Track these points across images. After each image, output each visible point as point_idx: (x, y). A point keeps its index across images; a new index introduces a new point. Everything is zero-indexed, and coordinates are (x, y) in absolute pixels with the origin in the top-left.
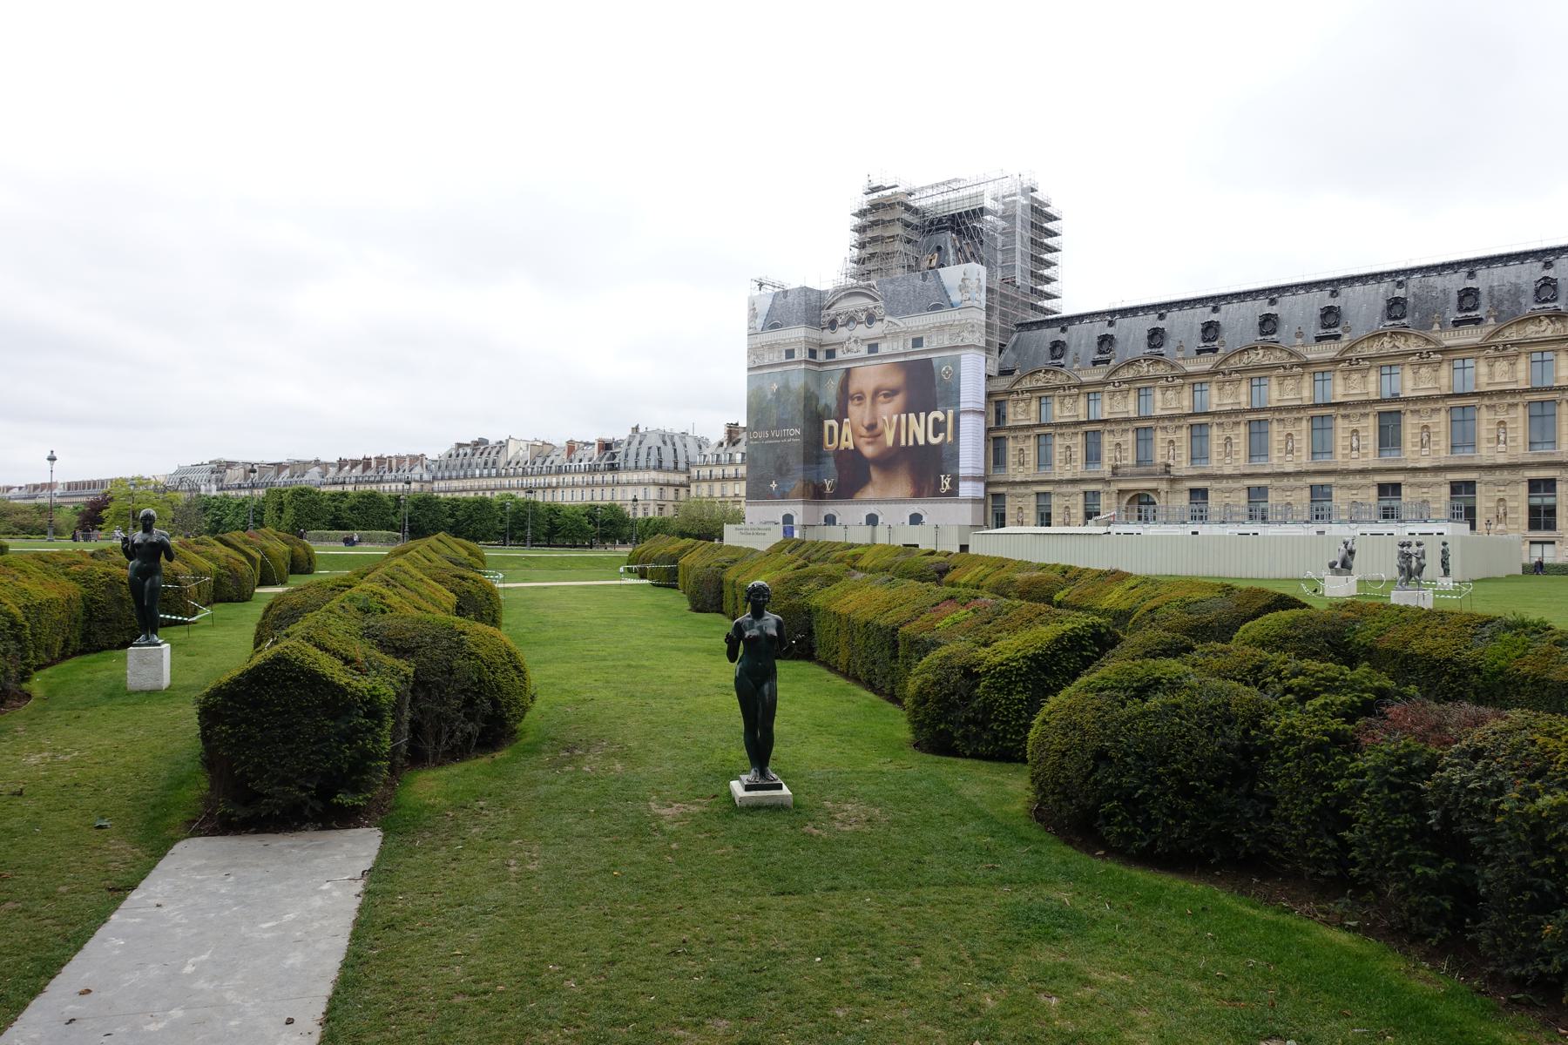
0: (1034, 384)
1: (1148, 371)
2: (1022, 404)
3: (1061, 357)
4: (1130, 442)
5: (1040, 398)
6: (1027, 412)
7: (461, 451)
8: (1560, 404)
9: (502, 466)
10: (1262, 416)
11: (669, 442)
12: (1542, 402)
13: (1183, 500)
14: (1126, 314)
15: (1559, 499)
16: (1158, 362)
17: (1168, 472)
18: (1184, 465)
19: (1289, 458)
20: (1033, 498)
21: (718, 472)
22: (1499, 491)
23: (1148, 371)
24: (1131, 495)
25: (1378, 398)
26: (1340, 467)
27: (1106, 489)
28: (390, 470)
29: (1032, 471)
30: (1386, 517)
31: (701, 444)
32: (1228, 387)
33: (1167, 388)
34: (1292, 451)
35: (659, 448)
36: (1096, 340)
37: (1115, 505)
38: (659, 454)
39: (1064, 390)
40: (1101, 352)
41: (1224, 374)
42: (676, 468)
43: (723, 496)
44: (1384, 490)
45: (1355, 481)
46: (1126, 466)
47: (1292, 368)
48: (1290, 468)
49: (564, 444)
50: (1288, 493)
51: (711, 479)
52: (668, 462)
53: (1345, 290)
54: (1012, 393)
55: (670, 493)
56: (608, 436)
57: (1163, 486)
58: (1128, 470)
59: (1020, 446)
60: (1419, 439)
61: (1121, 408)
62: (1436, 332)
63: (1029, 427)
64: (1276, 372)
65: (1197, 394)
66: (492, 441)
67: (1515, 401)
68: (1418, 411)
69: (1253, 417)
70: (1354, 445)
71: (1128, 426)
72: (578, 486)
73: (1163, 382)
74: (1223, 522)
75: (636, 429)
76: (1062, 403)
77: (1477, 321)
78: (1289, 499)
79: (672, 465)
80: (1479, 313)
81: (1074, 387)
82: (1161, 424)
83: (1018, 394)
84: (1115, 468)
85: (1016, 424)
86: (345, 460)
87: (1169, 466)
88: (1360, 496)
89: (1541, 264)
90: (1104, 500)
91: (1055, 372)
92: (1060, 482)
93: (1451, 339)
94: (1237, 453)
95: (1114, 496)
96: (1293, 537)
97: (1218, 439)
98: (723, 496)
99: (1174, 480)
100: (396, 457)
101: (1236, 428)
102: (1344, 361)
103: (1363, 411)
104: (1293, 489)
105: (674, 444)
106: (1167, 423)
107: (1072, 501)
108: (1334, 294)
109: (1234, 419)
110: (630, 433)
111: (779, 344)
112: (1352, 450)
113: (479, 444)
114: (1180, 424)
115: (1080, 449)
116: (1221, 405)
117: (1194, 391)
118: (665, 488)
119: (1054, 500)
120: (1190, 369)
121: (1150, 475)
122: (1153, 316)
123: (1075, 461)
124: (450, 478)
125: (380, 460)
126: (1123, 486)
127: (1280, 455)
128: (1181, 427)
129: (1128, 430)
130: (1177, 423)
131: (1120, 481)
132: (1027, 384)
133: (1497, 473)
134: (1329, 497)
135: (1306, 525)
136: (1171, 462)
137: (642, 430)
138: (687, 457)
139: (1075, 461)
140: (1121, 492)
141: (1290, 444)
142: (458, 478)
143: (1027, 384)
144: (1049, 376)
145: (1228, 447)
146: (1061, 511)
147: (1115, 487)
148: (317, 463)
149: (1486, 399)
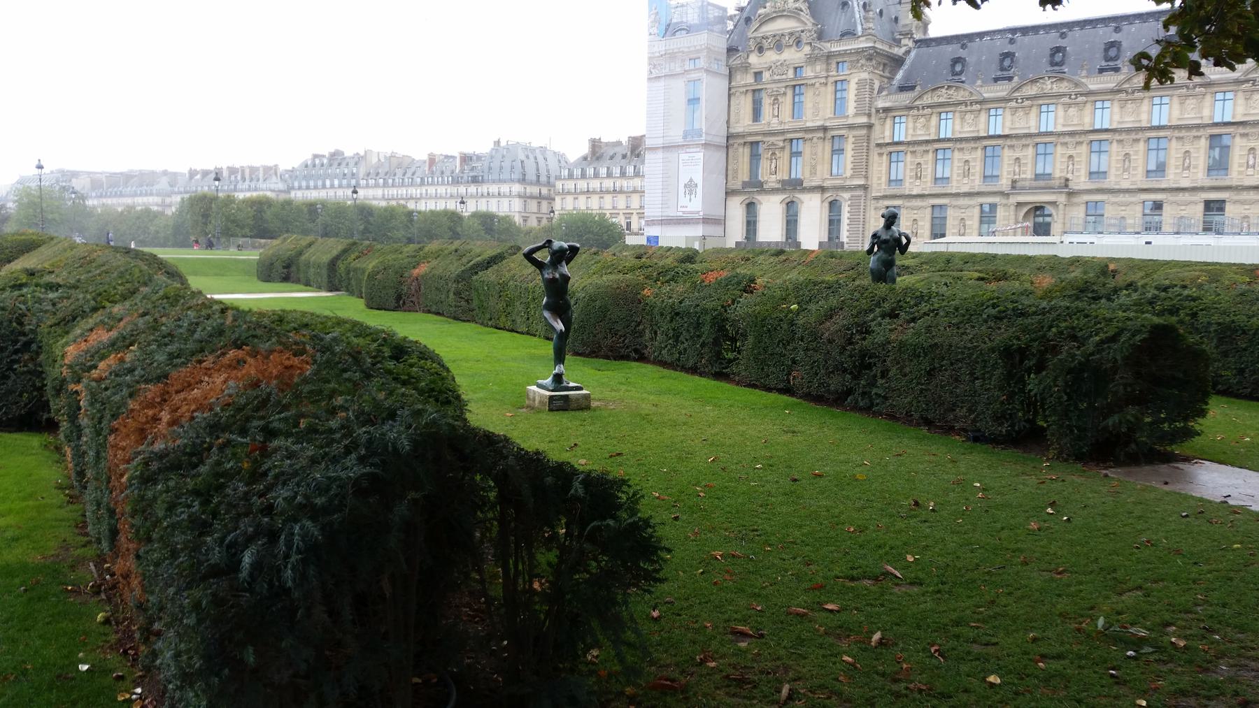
0: (936, 100)
1: (1052, 89)
2: (922, 120)
3: (961, 73)
4: (1030, 157)
5: (940, 113)
6: (926, 126)
7: (317, 161)
8: (1170, 140)
9: (361, 176)
10: (1162, 134)
11: (531, 157)
12: (1046, 143)
13: (1078, 213)
14: (1027, 32)
15: (1163, 218)
16: (1062, 79)
17: (1066, 186)
18: (1083, 179)
19: (1186, 173)
20: (929, 209)
21: (582, 185)
22: (1181, 210)
23: (1052, 89)
24: (1029, 207)
25: (1091, 129)
26: (1234, 183)
27: (1004, 201)
28: (244, 179)
29: (929, 184)
30: (1146, 230)
31: (560, 158)
32: (1130, 106)
33: (1070, 105)
34: (1188, 168)
35: (522, 162)
36: (1103, 47)
37: (1013, 217)
38: (523, 167)
39: (966, 106)
40: (1002, 69)
41: (1127, 92)
42: (538, 180)
43: (614, 208)
44: (1209, 206)
45: (1124, 199)
46: (1025, 180)
47: (1133, 92)
48: (1185, 183)
49: (425, 158)
50: (1183, 207)
51: (576, 193)
52: (531, 176)
53: (1125, 27)
54: (1011, 100)
55: (533, 205)
56: (469, 150)
57: (1062, 199)
58: (1027, 184)
59: (918, 160)
60: (1245, 161)
61: (1023, 124)
62: (1083, 77)
63: (927, 142)
64: (958, 108)
65: (1098, 112)
66: (348, 153)
67: (1199, 134)
68: (962, 149)
69: (1216, 131)
70: (1251, 163)
71: (1028, 141)
72: (441, 197)
73: (1066, 100)
74: (1177, 233)
75: (498, 143)
76: (962, 119)
77: (1117, 70)
78: (1247, 212)
79: (534, 178)
80: (1119, 63)
81: (977, 103)
82: (1062, 140)
83: (918, 109)
84: (1014, 182)
85: (1120, 126)
86: (195, 170)
87: (1067, 180)
88: (1187, 211)
89: (959, 45)
90: (1000, 213)
91: (957, 87)
92: (957, 195)
93: (1094, 84)
94: (1135, 168)
95: (1013, 208)
96: (1248, 247)
97: (1117, 156)
98: (614, 208)
99: (1071, 194)
100: (249, 167)
101: (1025, 150)
102: (1247, 81)
103: (1135, 137)
104: (1188, 204)
105: (536, 158)
106: (1067, 139)
107: (968, 213)
108: (1063, 36)
109: (1134, 136)
110: (492, 146)
111: (683, 52)
112: (1248, 167)
113: (336, 158)
114: (1081, 140)
115: (978, 163)
116: (1123, 122)
117: (940, 120)
118: (529, 200)
119: (950, 213)
120: (1092, 87)
121: (1048, 189)
122: (1054, 34)
123: (973, 175)
124: (308, 188)
125: (233, 171)
126: (1021, 199)
127: (1178, 171)
128: (1081, 143)
129: (1028, 145)
130: (1078, 139)
131: (1019, 194)
132: (927, 99)
133: (1181, 194)
134: (1221, 209)
135: (1136, 236)
136: (1069, 176)
137: (503, 144)
138: (548, 171)
139: (973, 175)
140: (1019, 205)
141: (1187, 161)
142: (316, 188)
143: (927, 99)
144: (951, 92)
145: (1127, 163)
146: (956, 222)
147: (1014, 200)
148: (165, 173)
149: (1117, 134)
